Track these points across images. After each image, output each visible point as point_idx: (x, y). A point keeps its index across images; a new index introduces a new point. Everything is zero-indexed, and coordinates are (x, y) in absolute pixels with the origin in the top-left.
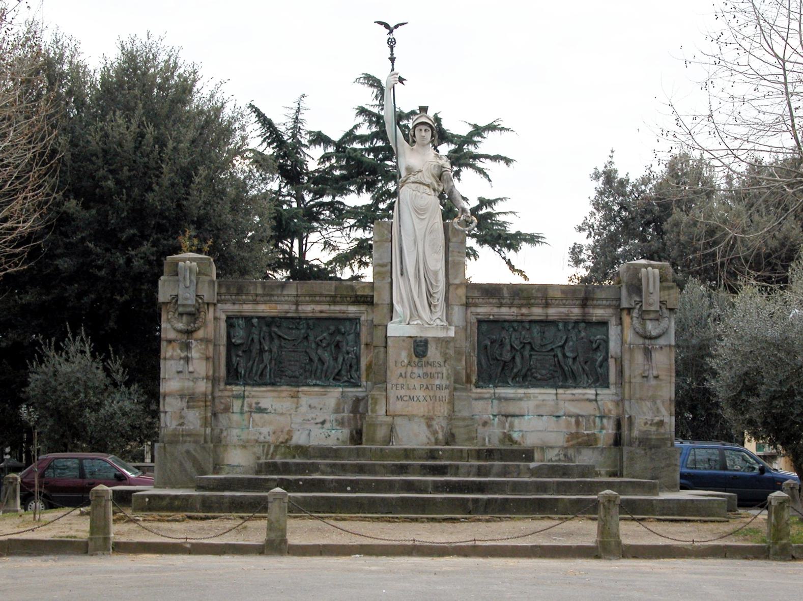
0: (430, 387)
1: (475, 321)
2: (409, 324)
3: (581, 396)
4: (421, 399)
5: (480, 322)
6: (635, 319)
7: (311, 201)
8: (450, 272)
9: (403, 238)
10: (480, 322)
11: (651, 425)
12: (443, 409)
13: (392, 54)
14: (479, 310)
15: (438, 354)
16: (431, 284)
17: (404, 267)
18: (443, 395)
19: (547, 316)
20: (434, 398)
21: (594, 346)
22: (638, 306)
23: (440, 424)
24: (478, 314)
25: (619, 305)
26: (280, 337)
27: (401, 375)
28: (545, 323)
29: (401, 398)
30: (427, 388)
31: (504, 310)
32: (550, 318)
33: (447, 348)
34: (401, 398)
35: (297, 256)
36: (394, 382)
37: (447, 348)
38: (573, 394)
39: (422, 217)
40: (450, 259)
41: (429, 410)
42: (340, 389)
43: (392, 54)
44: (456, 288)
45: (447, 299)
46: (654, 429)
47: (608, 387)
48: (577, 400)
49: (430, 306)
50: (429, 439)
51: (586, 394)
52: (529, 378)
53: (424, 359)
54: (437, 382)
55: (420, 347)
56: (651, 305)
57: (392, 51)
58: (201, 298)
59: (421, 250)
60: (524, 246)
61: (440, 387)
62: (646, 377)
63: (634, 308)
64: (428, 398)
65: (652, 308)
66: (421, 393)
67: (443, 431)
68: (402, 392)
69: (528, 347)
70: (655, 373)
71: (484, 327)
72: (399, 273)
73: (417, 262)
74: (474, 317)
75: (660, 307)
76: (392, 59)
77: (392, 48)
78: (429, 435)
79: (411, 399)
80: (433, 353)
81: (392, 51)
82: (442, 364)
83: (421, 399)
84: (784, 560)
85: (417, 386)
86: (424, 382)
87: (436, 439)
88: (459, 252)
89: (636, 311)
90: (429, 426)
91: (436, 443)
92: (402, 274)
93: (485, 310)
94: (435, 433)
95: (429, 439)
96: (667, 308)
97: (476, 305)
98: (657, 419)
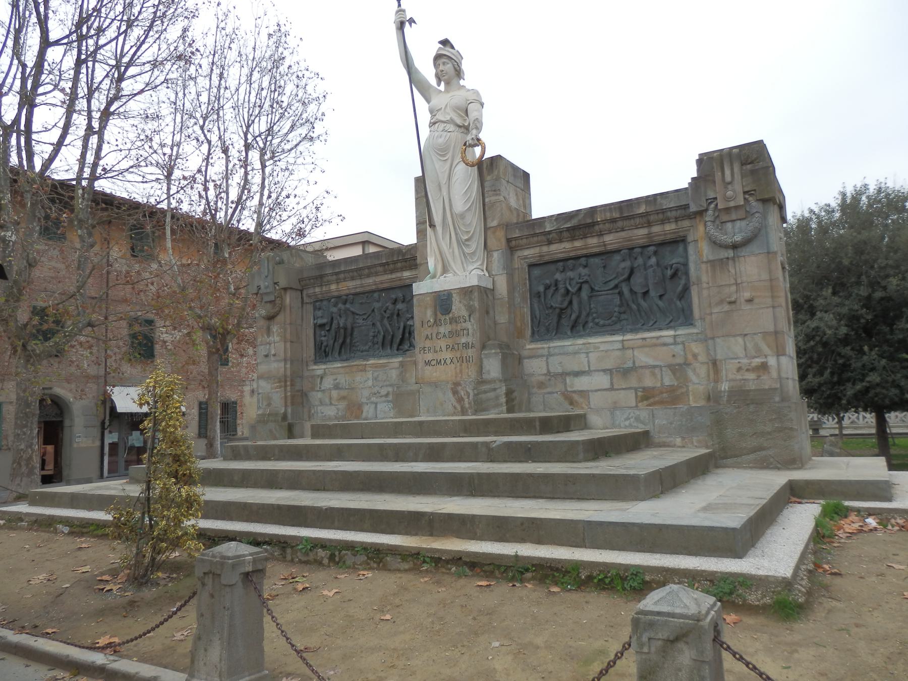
3: (654, 341)
4: (448, 361)
6: (709, 224)
8: (488, 213)
10: (531, 266)
11: (748, 370)
12: (471, 373)
14: (526, 253)
15: (463, 308)
18: (470, 354)
19: (605, 245)
20: (461, 359)
21: (669, 272)
23: (468, 390)
24: (526, 258)
26: (353, 313)
27: (427, 337)
28: (606, 254)
29: (428, 363)
31: (554, 247)
32: (609, 248)
33: (471, 299)
34: (428, 363)
36: (422, 345)
37: (471, 299)
41: (456, 373)
42: (401, 359)
44: (494, 233)
46: (751, 376)
48: (652, 348)
50: (455, 408)
52: (591, 324)
54: (463, 340)
60: (496, 141)
61: (466, 346)
62: (734, 302)
63: (706, 210)
64: (455, 360)
66: (448, 355)
67: (468, 398)
68: (429, 356)
69: (585, 287)
70: (747, 295)
71: (536, 272)
78: (455, 403)
79: (439, 362)
80: (458, 308)
82: (467, 319)
83: (448, 361)
85: (444, 348)
86: (450, 342)
87: (462, 408)
89: (710, 212)
90: (455, 393)
91: (464, 412)
94: (460, 400)
95: (455, 408)
97: (522, 248)
98: (757, 361)
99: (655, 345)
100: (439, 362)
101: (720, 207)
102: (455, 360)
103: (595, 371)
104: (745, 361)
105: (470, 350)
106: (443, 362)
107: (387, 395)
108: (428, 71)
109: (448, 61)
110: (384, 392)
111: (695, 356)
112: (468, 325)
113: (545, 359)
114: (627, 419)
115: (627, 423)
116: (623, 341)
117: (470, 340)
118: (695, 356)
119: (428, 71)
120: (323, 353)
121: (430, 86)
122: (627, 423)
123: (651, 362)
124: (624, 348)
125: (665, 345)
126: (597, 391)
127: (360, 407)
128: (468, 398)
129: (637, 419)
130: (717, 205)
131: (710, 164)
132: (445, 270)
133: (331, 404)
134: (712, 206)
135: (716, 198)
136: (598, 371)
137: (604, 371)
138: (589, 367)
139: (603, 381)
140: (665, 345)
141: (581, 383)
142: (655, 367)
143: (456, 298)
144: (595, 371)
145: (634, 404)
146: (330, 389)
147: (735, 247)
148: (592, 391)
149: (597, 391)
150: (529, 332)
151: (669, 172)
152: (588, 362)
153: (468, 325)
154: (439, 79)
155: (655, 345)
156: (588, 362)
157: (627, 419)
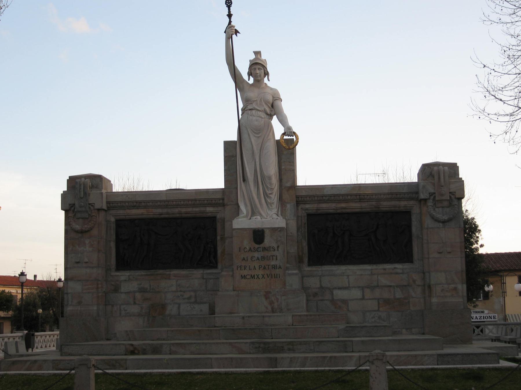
0: (267, 267)
1: (305, 214)
2: (250, 219)
4: (260, 276)
5: (309, 215)
7: (211, 279)
9: (243, 153)
10: (309, 215)
13: (229, 12)
14: (307, 206)
16: (267, 187)
17: (245, 173)
22: (432, 197)
25: (418, 197)
27: (244, 259)
29: (243, 277)
30: (265, 268)
34: (243, 277)
35: (517, 365)
38: (385, 269)
39: (258, 136)
40: (283, 167)
43: (229, 12)
45: (281, 198)
47: (412, 262)
48: (387, 275)
49: (267, 205)
50: (267, 308)
51: (395, 268)
53: (262, 245)
54: (273, 263)
55: (258, 235)
56: (442, 195)
57: (229, 9)
58: (92, 206)
59: (257, 160)
63: (429, 199)
64: (265, 276)
65: (444, 198)
66: (260, 272)
68: (245, 272)
72: (242, 179)
73: (256, 171)
74: (303, 211)
75: (450, 197)
76: (230, 16)
77: (229, 7)
79: (253, 277)
80: (268, 241)
81: (229, 9)
83: (260, 276)
84: (331, 265)
85: (257, 267)
87: (272, 308)
88: (290, 162)
92: (244, 180)
93: (311, 207)
95: (267, 308)
96: (456, 198)
97: (305, 203)
99: (391, 273)
100: (253, 277)
101: (437, 199)
102: (265, 276)
103: (353, 287)
104: (446, 286)
105: (278, 270)
106: (256, 277)
107: (189, 298)
108: (243, 68)
109: (258, 67)
110: (187, 295)
111: (414, 281)
112: (276, 253)
113: (319, 278)
114: (373, 318)
115: (373, 320)
116: (372, 269)
117: (277, 263)
118: (414, 281)
119: (243, 68)
120: (123, 263)
121: (244, 80)
122: (373, 320)
123: (389, 283)
124: (372, 274)
125: (397, 273)
126: (353, 300)
127: (163, 307)
128: (278, 302)
129: (380, 318)
130: (435, 197)
131: (429, 171)
132: (253, 214)
133: (135, 303)
134: (432, 197)
135: (435, 193)
136: (355, 287)
137: (359, 287)
138: (349, 284)
139: (356, 293)
140: (397, 273)
141: (339, 294)
142: (391, 286)
143: (267, 234)
144: (353, 287)
145: (377, 308)
146: (134, 292)
147: (444, 222)
148: (350, 300)
149: (353, 300)
150: (306, 260)
151: (405, 171)
152: (349, 280)
153: (276, 253)
154: (250, 74)
155: (391, 273)
156: (349, 280)
157: (373, 318)
